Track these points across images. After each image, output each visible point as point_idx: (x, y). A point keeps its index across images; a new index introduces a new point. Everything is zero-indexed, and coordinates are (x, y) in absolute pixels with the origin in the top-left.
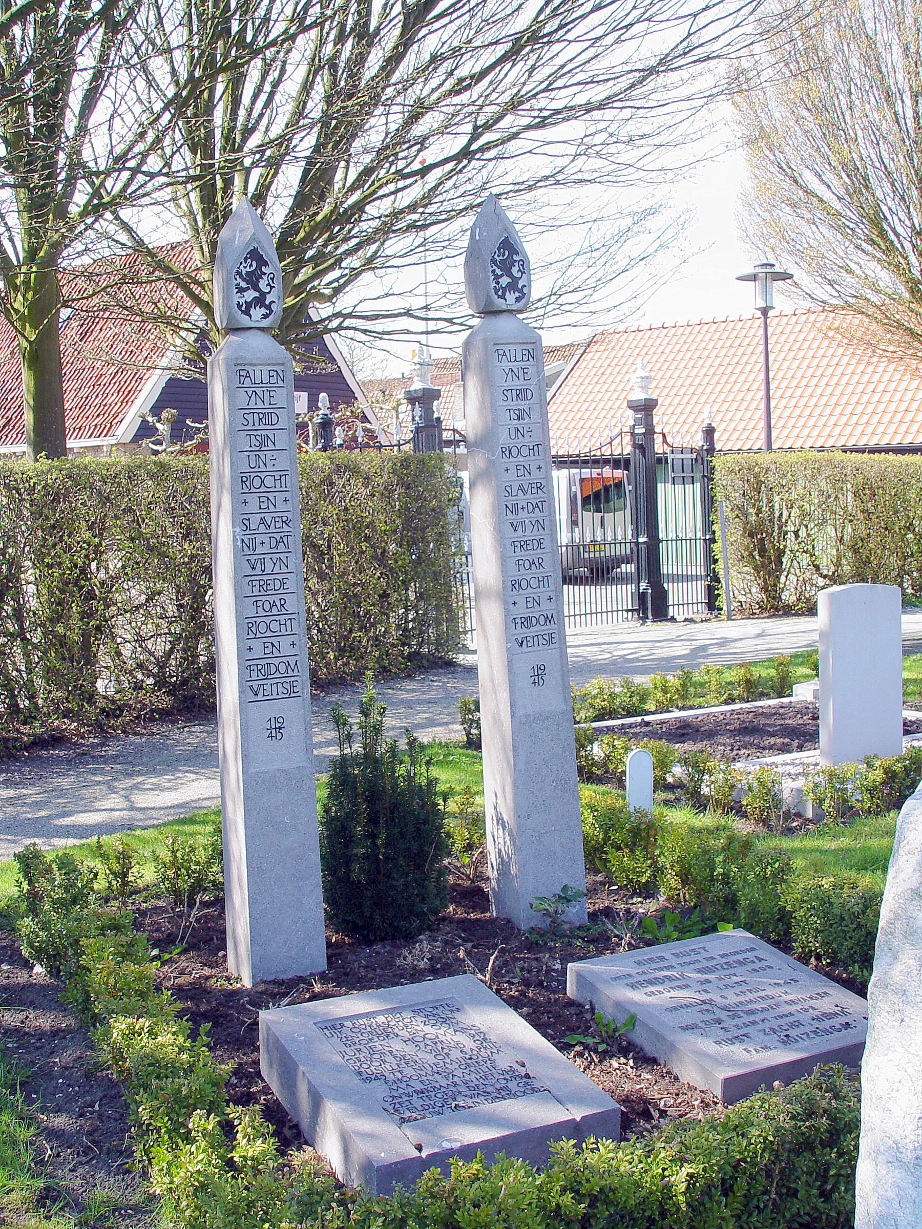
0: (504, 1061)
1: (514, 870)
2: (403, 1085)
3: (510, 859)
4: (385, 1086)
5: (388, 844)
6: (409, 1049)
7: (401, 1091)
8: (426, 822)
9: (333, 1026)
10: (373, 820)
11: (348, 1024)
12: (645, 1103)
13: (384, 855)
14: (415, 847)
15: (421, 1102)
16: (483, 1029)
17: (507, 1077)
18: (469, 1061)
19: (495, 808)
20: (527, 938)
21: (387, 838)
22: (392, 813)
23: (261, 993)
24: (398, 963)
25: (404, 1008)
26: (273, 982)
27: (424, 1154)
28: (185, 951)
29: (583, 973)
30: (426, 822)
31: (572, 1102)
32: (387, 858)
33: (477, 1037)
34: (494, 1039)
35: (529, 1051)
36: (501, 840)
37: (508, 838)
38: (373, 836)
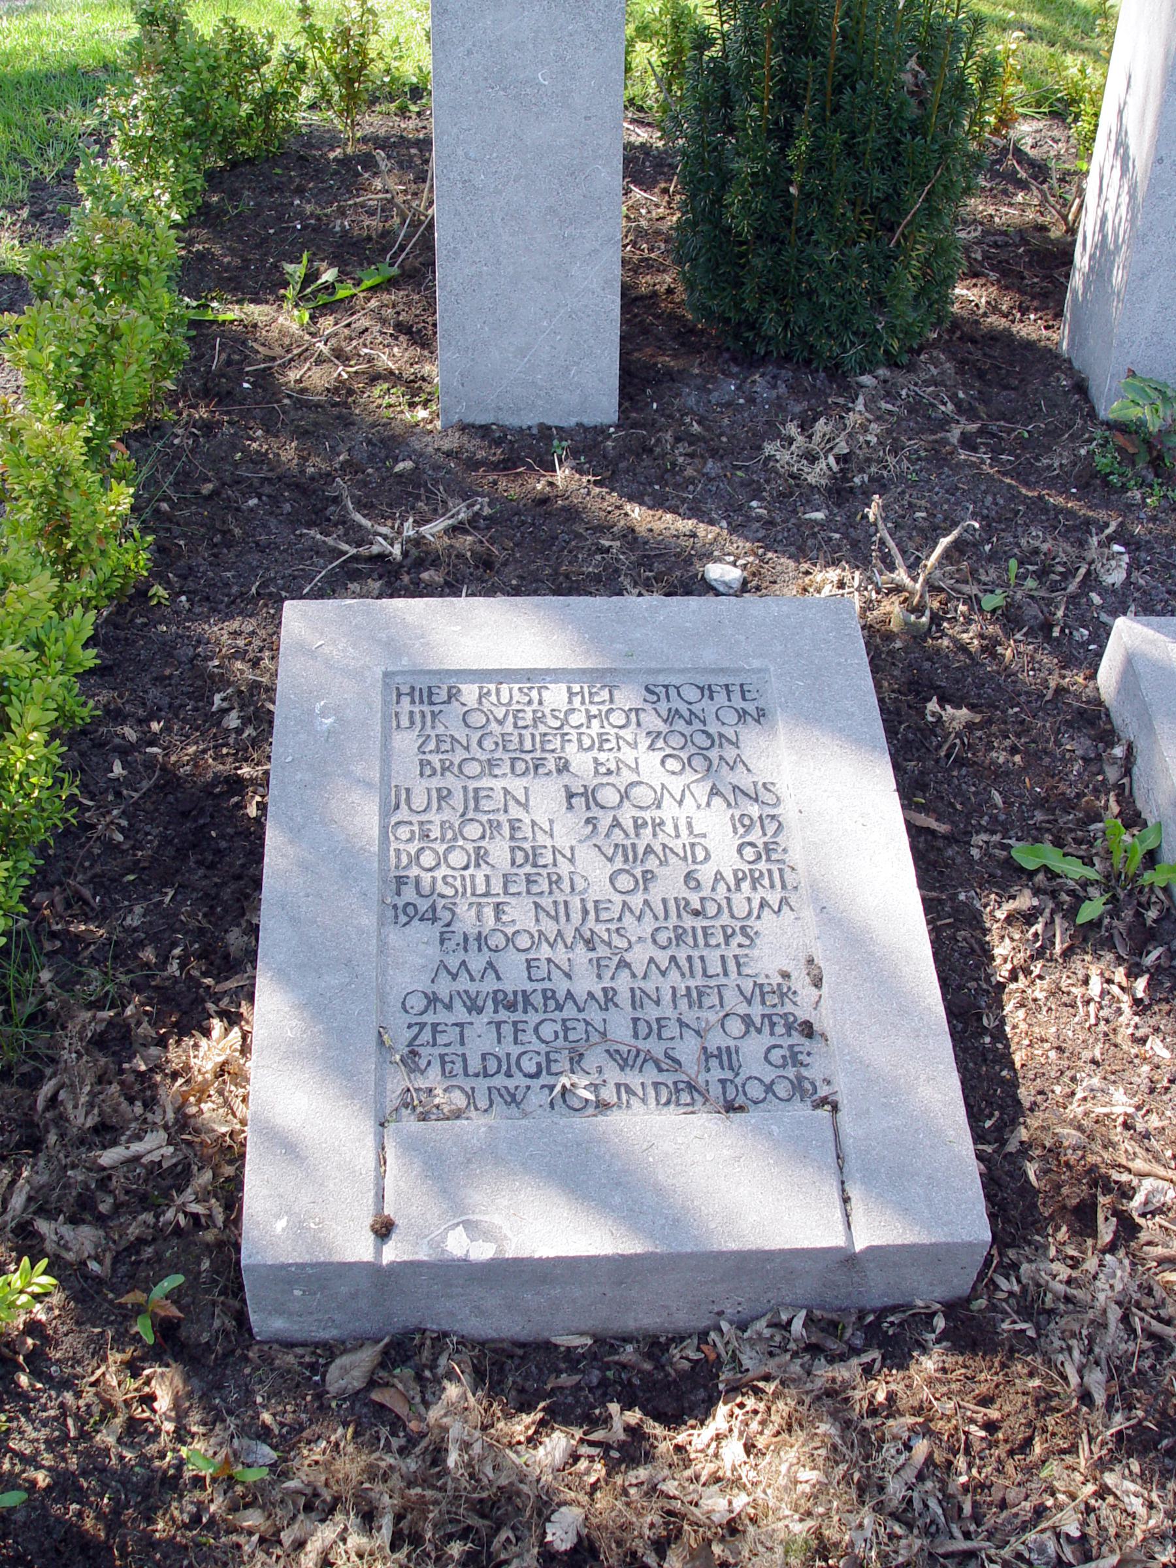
0: (778, 947)
1: (1118, 277)
2: (477, 963)
3: (1118, 248)
4: (433, 951)
5: (814, 164)
6: (566, 830)
7: (463, 983)
8: (917, 128)
9: (425, 694)
10: (789, 94)
11: (469, 693)
12: (1094, 1184)
13: (801, 187)
14: (879, 184)
15: (488, 1042)
16: (787, 812)
17: (756, 1011)
18: (693, 924)
19: (1120, 112)
20: (1090, 454)
21: (812, 150)
22: (838, 89)
23: (448, 454)
24: (769, 448)
25: (629, 674)
26: (484, 431)
27: (391, 1253)
28: (391, 283)
29: (1140, 668)
30: (917, 128)
31: (869, 1178)
32: (807, 196)
33: (755, 836)
34: (796, 856)
35: (855, 941)
36: (1112, 195)
37: (1125, 199)
38: (785, 135)
